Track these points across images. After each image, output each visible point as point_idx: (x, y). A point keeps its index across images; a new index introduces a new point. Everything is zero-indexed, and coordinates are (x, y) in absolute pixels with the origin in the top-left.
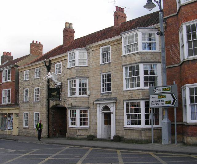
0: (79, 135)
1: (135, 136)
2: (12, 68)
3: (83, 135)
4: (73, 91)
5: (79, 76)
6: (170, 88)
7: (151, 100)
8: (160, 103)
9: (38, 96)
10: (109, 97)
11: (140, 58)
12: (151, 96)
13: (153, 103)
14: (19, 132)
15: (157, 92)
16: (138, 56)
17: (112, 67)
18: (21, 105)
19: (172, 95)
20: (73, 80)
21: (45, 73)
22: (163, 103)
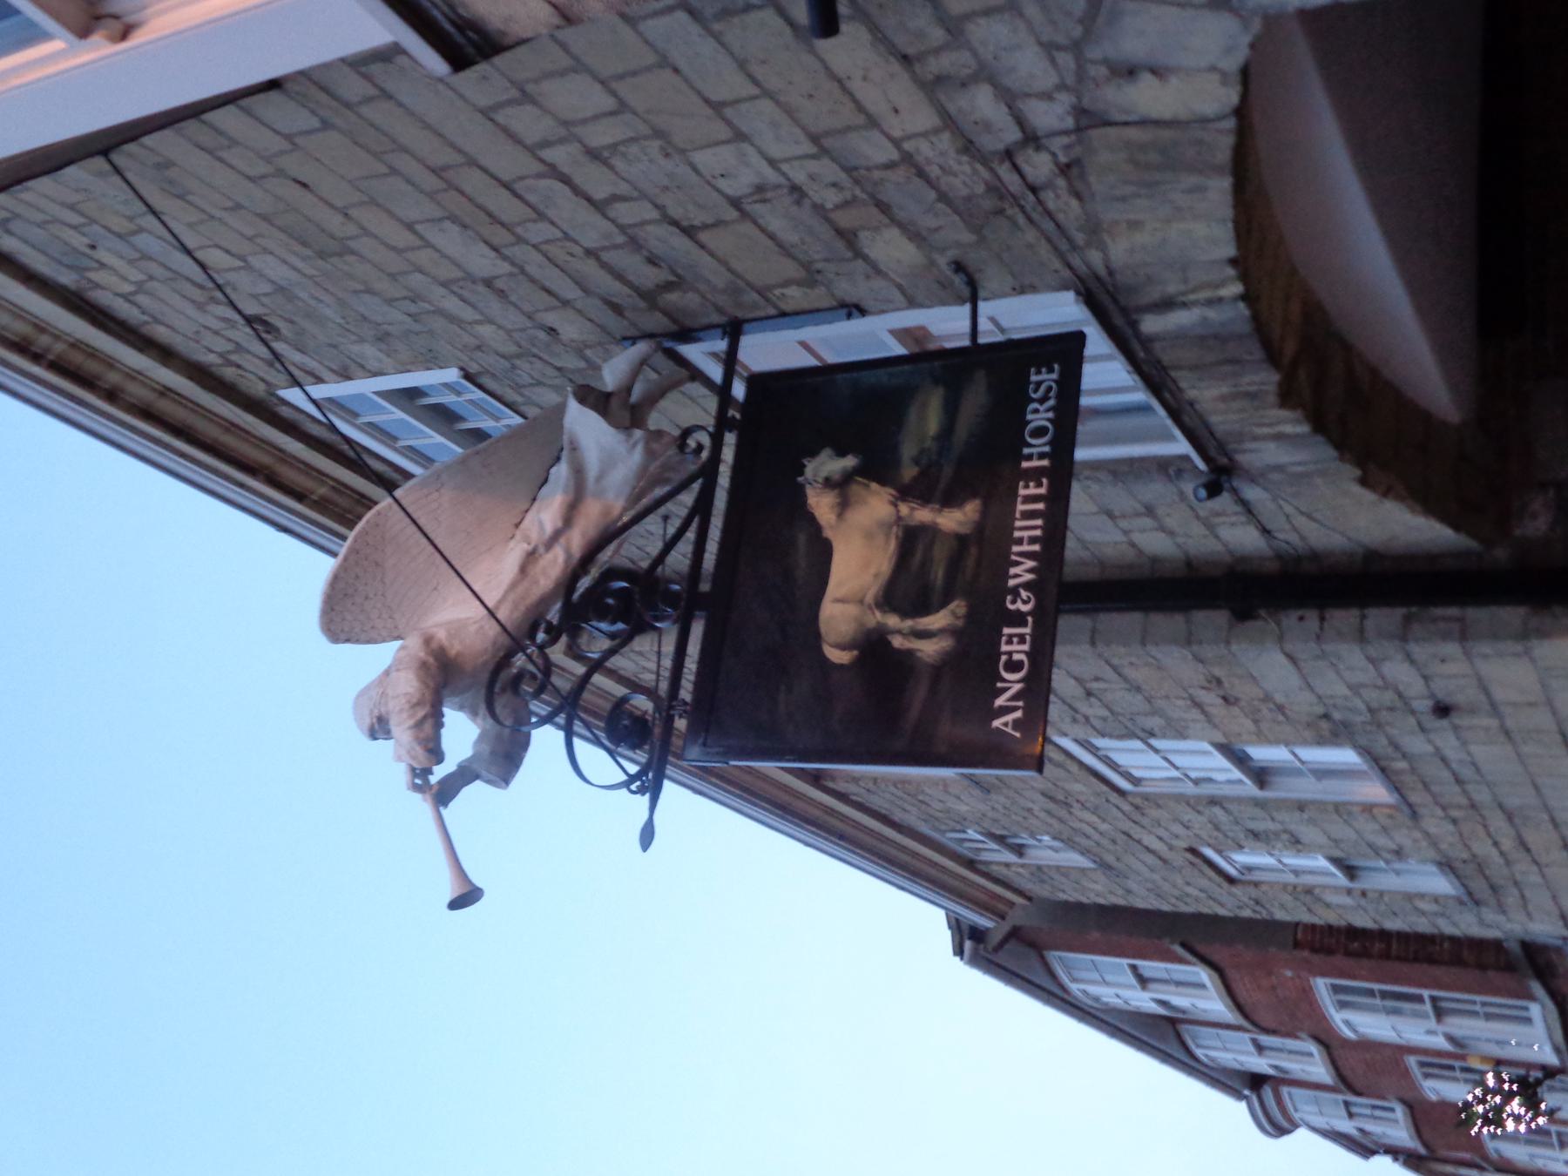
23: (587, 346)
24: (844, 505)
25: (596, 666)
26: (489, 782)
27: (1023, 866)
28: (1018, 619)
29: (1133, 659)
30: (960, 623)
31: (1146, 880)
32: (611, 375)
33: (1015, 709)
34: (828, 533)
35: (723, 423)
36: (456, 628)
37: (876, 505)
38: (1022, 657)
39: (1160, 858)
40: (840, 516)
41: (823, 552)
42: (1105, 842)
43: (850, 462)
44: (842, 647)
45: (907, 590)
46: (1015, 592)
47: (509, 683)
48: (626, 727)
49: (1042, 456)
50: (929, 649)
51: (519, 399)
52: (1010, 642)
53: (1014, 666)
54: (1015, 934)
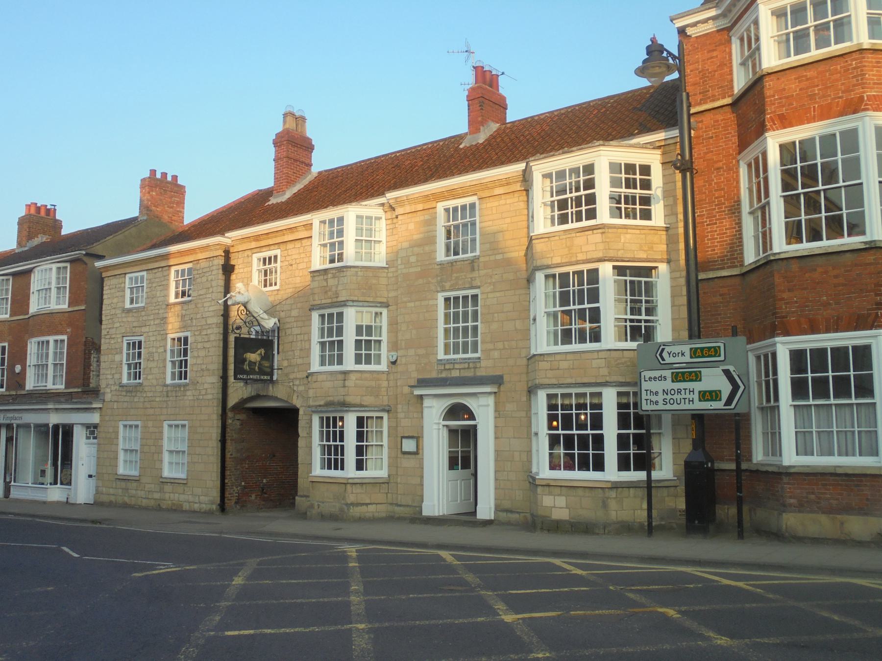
0: (352, 504)
1: (588, 510)
2: (72, 261)
3: (367, 504)
4: (333, 349)
5: (356, 298)
6: (719, 347)
7: (645, 385)
8: (679, 396)
9: (184, 364)
10: (469, 374)
11: (601, 246)
12: (648, 374)
13: (654, 398)
14: (98, 492)
15: (668, 360)
16: (596, 237)
17: (482, 272)
18: (108, 397)
19: (727, 373)
20: (335, 311)
21: (214, 284)
22: (691, 396)
37: (258, 359)
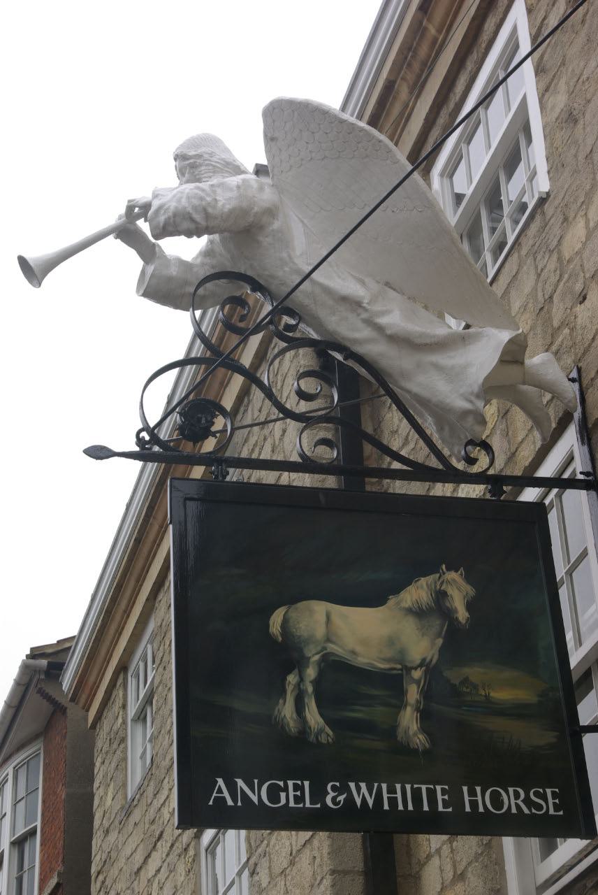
23: (572, 330)
24: (418, 613)
25: (251, 377)
26: (143, 273)
27: (124, 722)
28: (318, 794)
29: (318, 860)
30: (312, 738)
31: (119, 852)
32: (537, 360)
33: (234, 799)
34: (392, 601)
35: (496, 482)
36: (284, 240)
37: (421, 646)
38: (283, 801)
39: (139, 869)
40: (410, 611)
41: (373, 598)
42: (152, 811)
43: (462, 615)
44: (285, 621)
45: (343, 681)
46: (344, 789)
47: (237, 291)
48: (199, 420)
49: (474, 804)
50: (287, 710)
51: (524, 252)
52: (296, 787)
53: (274, 794)
54: (58, 710)
